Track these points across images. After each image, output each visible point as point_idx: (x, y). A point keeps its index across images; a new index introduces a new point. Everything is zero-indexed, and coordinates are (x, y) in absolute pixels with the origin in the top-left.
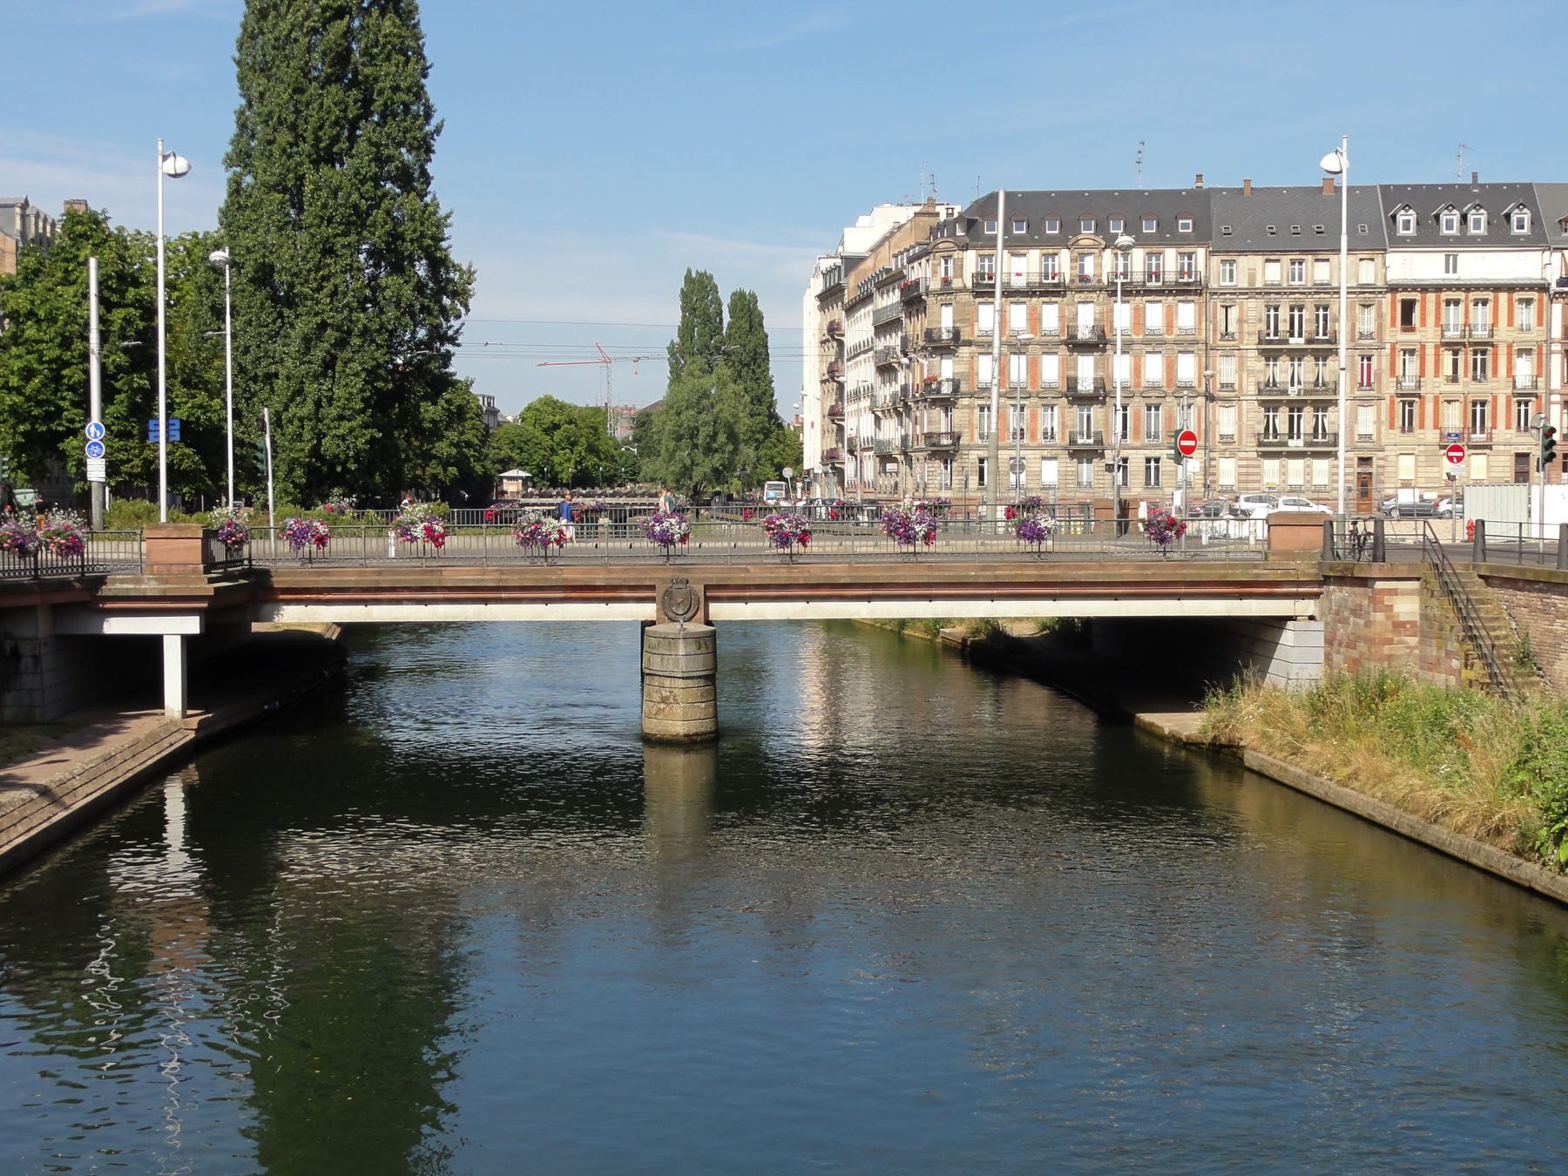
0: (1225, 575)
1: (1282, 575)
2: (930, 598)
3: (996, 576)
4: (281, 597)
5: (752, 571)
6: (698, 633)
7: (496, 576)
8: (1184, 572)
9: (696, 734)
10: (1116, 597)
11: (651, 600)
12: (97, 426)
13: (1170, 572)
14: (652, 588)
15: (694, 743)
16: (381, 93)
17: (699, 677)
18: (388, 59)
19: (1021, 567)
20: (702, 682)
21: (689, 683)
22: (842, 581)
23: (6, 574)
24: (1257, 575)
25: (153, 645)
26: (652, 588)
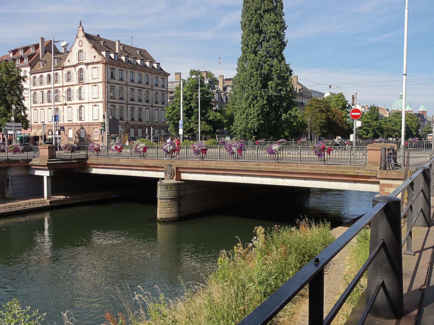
0: (344, 172)
1: (369, 173)
2: (242, 175)
3: (259, 168)
4: (91, 166)
5: (190, 163)
6: (167, 184)
7: (39, 162)
8: (329, 169)
9: (165, 219)
10: (305, 179)
11: (162, 171)
12: (181, 121)
13: (323, 169)
14: (163, 167)
15: (164, 221)
16: (268, 34)
17: (168, 199)
18: (270, 25)
19: (269, 165)
20: (169, 201)
21: (166, 201)
22: (212, 168)
23: (65, 157)
24: (358, 173)
25: (42, 177)
26: (163, 167)
